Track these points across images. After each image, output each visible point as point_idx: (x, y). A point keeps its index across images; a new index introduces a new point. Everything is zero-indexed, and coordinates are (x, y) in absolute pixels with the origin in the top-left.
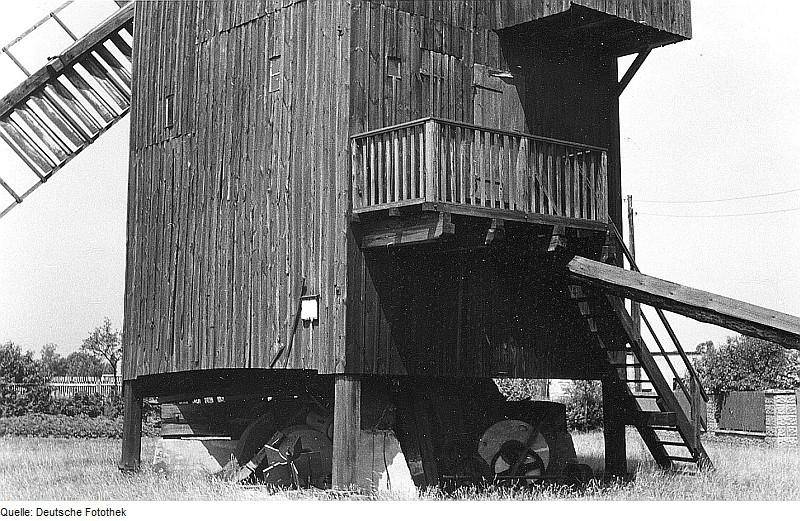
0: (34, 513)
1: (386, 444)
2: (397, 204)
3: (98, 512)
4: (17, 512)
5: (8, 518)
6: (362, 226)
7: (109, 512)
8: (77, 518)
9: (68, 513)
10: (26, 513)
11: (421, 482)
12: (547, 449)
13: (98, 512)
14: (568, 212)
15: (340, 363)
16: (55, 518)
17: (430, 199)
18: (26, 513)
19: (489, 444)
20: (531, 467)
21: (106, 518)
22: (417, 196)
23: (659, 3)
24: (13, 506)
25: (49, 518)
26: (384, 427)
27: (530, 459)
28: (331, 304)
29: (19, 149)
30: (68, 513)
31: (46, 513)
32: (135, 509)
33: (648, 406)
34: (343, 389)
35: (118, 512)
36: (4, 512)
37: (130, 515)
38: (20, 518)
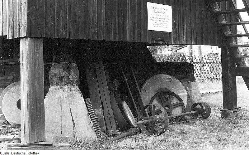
0: (10, 153)
1: (70, 98)
4: (5, 153)
7: (34, 153)
9: (21, 154)
10: (8, 153)
13: (30, 153)
18: (8, 153)
19: (147, 94)
20: (176, 106)
30: (21, 154)
31: (14, 153)
35: (37, 153)
36: (1, 153)
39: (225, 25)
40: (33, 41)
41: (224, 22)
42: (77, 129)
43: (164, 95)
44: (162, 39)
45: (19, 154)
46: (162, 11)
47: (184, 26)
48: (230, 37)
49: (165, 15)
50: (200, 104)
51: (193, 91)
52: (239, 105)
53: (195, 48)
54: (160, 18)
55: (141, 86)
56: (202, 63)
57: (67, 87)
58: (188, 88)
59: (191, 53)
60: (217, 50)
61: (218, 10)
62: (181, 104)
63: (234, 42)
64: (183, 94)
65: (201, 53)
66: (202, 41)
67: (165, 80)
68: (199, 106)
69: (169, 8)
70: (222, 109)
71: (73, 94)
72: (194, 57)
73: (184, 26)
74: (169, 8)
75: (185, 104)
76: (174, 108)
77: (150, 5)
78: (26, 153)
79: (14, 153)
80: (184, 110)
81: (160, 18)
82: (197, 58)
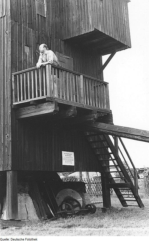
0: (10, 240)
1: (25, 199)
2: (33, 99)
3: (29, 239)
4: (5, 239)
5: (2, 241)
6: (16, 110)
7: (32, 239)
8: (23, 241)
9: (20, 240)
10: (8, 240)
11: (40, 214)
12: (82, 199)
13: (29, 239)
14: (72, 100)
15: (9, 166)
16: (16, 241)
17: (48, 95)
18: (8, 240)
19: (60, 199)
20: (76, 206)
21: (31, 241)
22: (43, 95)
23: (84, 2)
24: (4, 238)
25: (15, 241)
26: (25, 192)
27: (76, 204)
28: (4, 141)
29: (18, 87)
30: (20, 240)
31: (13, 240)
32: (40, 238)
33: (118, 181)
34: (9, 175)
35: (35, 239)
36: (1, 239)
37: (38, 240)
38: (6, 241)
39: (102, 161)
40: (78, 22)
41: (102, 159)
42: (29, 215)
43: (70, 200)
44: (70, 169)
45: (18, 240)
46: (69, 155)
47: (80, 162)
48: (105, 167)
49: (71, 157)
50: (90, 205)
51: (85, 199)
52: (112, 205)
53: (84, 173)
54: (68, 158)
55: (56, 196)
56: (89, 183)
57: (23, 194)
58: (83, 196)
59: (81, 177)
60: (99, 174)
61: (98, 153)
62: (79, 205)
63: (107, 170)
64: (80, 200)
65: (88, 177)
66: (88, 170)
67: (69, 192)
68: (89, 206)
69: (73, 153)
70: (103, 207)
71: (27, 197)
72: (83, 179)
73: (80, 162)
74: (73, 153)
75: (82, 205)
76: (75, 207)
77: (62, 152)
78: (25, 240)
79: (13, 240)
80: (81, 208)
81: (68, 158)
82: (86, 180)
